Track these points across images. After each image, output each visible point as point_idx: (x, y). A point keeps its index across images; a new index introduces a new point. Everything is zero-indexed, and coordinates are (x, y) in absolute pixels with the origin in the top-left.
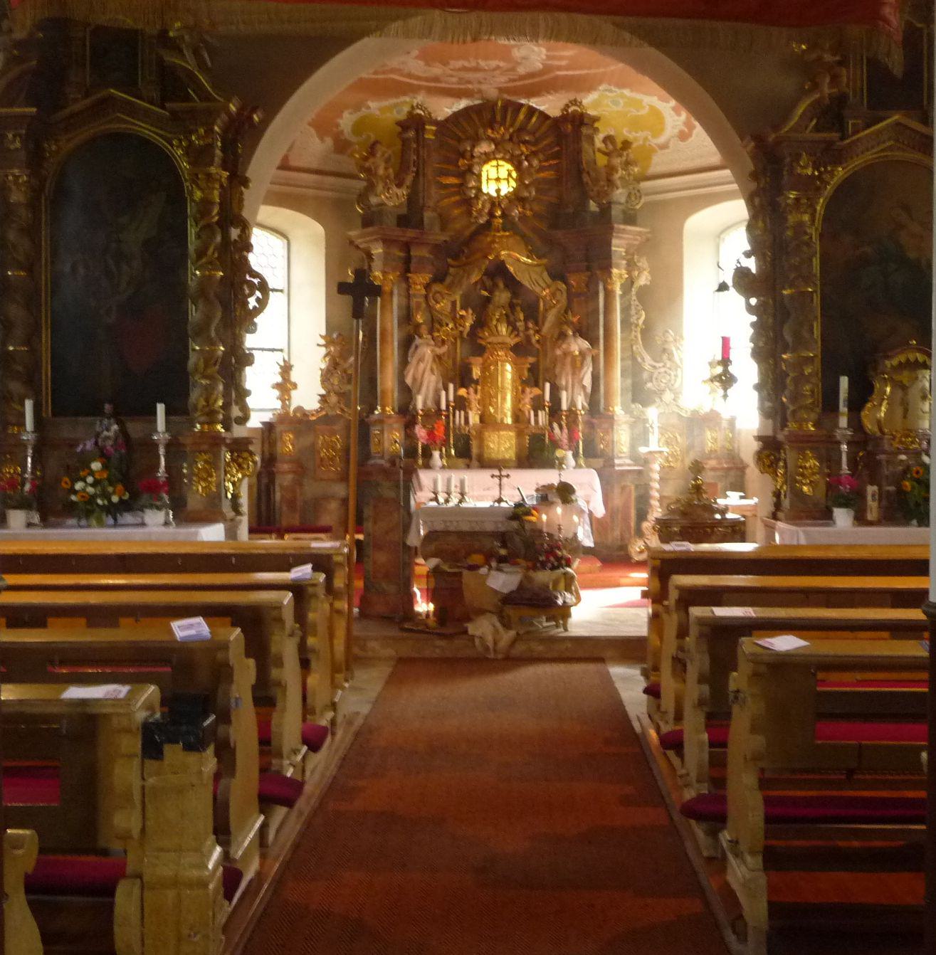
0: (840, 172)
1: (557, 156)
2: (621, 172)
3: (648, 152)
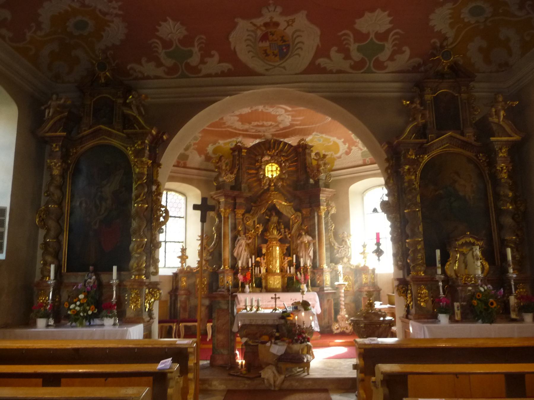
1: (296, 161)
2: (322, 168)
3: (333, 160)
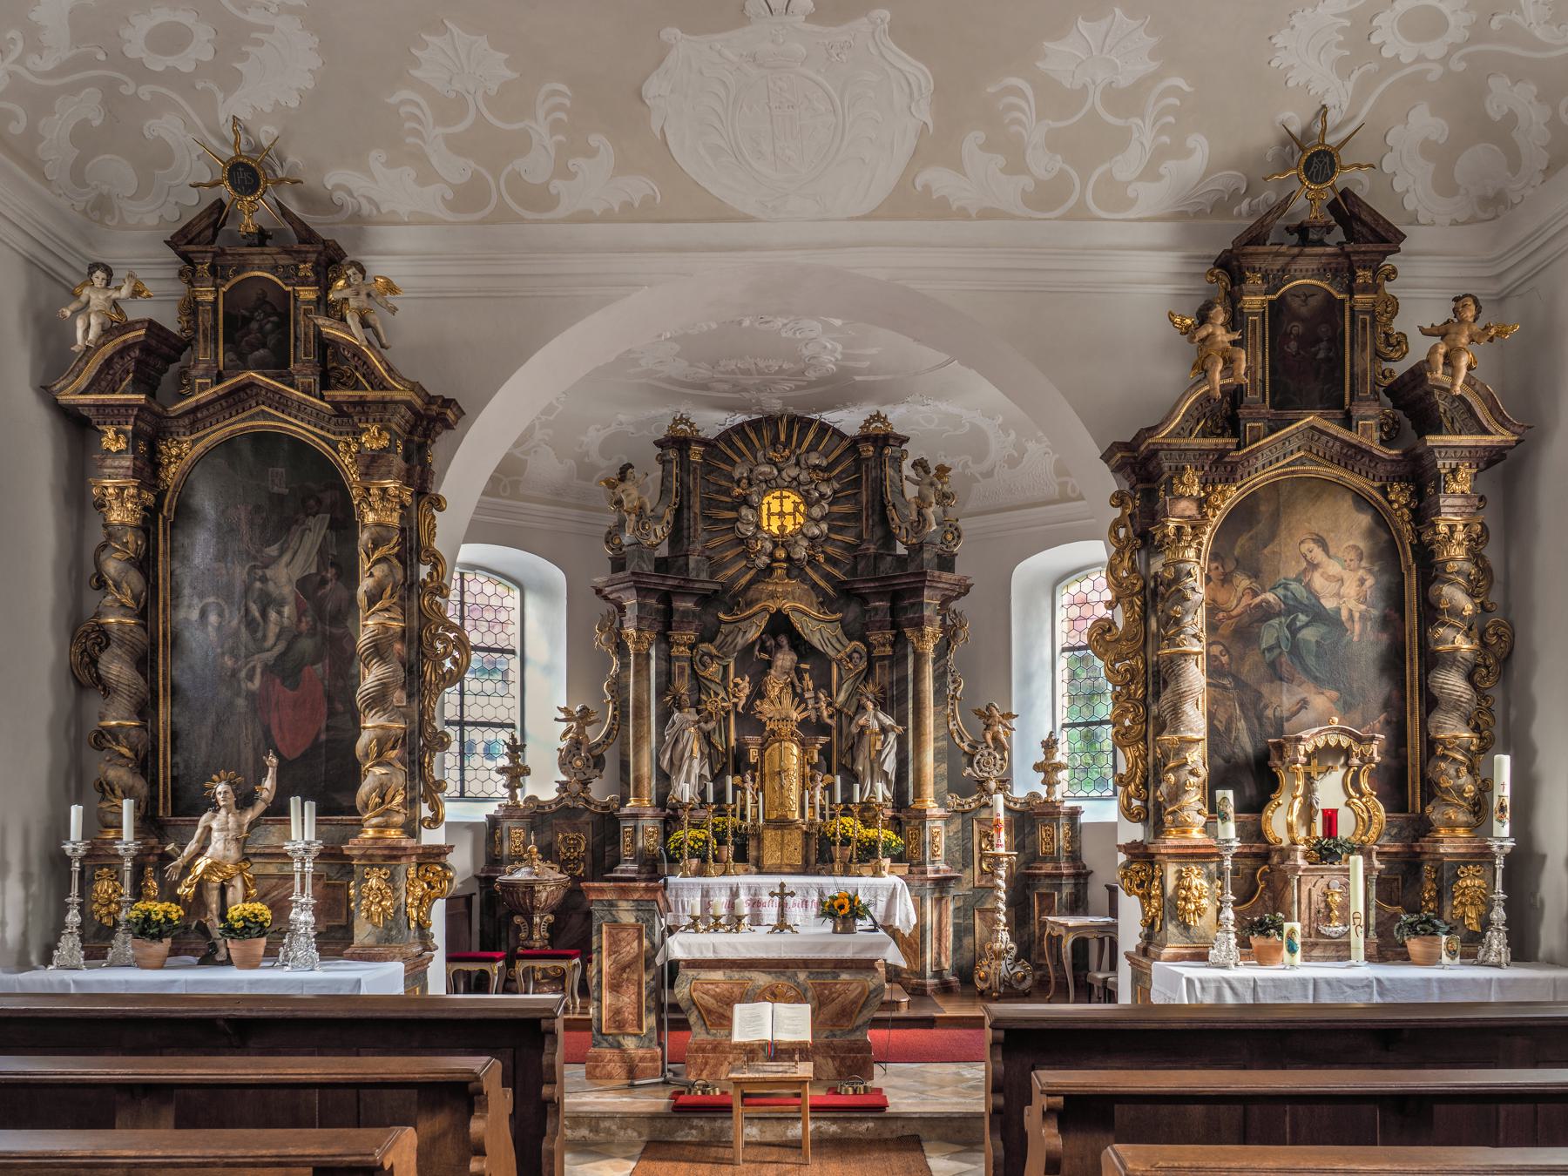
0: (1234, 494)
